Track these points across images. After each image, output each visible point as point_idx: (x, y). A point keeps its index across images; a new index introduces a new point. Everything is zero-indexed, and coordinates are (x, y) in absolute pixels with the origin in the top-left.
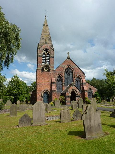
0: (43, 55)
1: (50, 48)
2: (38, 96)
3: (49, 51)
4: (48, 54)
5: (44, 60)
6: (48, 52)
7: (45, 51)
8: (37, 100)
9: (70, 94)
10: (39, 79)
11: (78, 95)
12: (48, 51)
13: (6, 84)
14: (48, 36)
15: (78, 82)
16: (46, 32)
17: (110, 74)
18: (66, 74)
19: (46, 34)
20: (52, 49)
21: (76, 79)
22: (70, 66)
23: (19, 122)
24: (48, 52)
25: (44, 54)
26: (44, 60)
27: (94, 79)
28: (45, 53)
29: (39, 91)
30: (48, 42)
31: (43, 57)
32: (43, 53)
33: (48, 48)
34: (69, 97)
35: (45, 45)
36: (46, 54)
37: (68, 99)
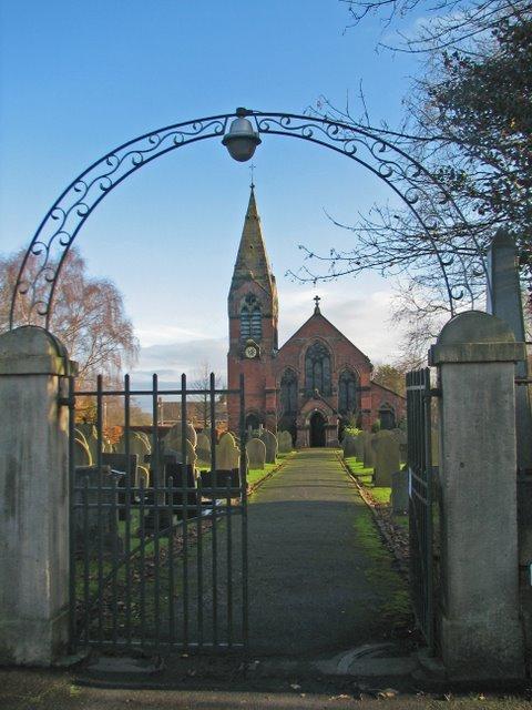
7: (247, 300)
9: (308, 422)
12: (254, 301)
15: (347, 384)
25: (245, 309)
33: (257, 291)
36: (250, 308)
37: (305, 435)
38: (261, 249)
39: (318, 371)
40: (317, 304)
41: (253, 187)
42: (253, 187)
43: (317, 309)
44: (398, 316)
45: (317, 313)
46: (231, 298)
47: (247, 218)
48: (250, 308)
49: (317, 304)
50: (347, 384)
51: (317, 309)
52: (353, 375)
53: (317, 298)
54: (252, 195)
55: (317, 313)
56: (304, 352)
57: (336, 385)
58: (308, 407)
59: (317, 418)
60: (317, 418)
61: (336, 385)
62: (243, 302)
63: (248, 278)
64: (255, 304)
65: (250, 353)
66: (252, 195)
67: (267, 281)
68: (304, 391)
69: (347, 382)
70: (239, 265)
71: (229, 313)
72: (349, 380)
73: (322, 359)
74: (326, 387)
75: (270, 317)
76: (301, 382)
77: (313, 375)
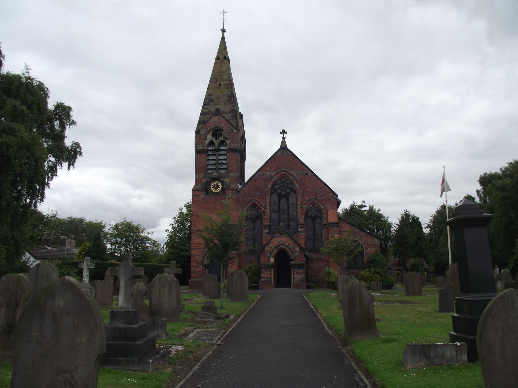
0: (209, 149)
1: (228, 125)
2: (193, 263)
3: (224, 133)
4: (222, 143)
5: (211, 162)
6: (221, 138)
7: (213, 135)
8: (192, 275)
9: (272, 260)
10: (197, 215)
11: (298, 262)
12: (221, 135)
13: (253, 164)
14: (226, 90)
15: (314, 221)
16: (222, 80)
17: (516, 162)
18: (275, 198)
19: (220, 85)
20: (233, 126)
21: (307, 213)
22: (286, 174)
23: (416, 346)
24: (222, 137)
25: (211, 143)
26: (211, 162)
27: (496, 173)
28: (214, 140)
29: (197, 250)
30: (222, 107)
31: (209, 153)
32: (207, 142)
33: (223, 125)
34: (269, 266)
35: (215, 119)
36: (217, 142)
37: (268, 275)
38: (230, 84)
39: (284, 206)
40: (284, 138)
41: (283, 132)
42: (224, 31)
43: (283, 143)
44: (171, 225)
45: (284, 148)
46: (198, 132)
47: (218, 58)
48: (217, 142)
49: (284, 138)
50: (314, 221)
51: (283, 143)
52: (319, 211)
53: (224, 13)
54: (223, 38)
55: (284, 148)
56: (269, 186)
57: (302, 222)
58: (274, 243)
59: (282, 256)
60: (282, 256)
61: (302, 222)
62: (209, 137)
63: (218, 112)
64: (221, 138)
65: (216, 188)
66: (223, 38)
67: (237, 118)
68: (269, 226)
69: (314, 218)
70: (208, 101)
71: (196, 147)
72: (316, 216)
73: (288, 194)
74: (292, 223)
75: (240, 152)
76: (266, 217)
77: (279, 211)
